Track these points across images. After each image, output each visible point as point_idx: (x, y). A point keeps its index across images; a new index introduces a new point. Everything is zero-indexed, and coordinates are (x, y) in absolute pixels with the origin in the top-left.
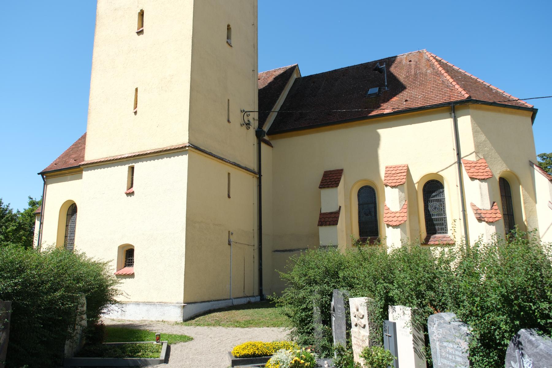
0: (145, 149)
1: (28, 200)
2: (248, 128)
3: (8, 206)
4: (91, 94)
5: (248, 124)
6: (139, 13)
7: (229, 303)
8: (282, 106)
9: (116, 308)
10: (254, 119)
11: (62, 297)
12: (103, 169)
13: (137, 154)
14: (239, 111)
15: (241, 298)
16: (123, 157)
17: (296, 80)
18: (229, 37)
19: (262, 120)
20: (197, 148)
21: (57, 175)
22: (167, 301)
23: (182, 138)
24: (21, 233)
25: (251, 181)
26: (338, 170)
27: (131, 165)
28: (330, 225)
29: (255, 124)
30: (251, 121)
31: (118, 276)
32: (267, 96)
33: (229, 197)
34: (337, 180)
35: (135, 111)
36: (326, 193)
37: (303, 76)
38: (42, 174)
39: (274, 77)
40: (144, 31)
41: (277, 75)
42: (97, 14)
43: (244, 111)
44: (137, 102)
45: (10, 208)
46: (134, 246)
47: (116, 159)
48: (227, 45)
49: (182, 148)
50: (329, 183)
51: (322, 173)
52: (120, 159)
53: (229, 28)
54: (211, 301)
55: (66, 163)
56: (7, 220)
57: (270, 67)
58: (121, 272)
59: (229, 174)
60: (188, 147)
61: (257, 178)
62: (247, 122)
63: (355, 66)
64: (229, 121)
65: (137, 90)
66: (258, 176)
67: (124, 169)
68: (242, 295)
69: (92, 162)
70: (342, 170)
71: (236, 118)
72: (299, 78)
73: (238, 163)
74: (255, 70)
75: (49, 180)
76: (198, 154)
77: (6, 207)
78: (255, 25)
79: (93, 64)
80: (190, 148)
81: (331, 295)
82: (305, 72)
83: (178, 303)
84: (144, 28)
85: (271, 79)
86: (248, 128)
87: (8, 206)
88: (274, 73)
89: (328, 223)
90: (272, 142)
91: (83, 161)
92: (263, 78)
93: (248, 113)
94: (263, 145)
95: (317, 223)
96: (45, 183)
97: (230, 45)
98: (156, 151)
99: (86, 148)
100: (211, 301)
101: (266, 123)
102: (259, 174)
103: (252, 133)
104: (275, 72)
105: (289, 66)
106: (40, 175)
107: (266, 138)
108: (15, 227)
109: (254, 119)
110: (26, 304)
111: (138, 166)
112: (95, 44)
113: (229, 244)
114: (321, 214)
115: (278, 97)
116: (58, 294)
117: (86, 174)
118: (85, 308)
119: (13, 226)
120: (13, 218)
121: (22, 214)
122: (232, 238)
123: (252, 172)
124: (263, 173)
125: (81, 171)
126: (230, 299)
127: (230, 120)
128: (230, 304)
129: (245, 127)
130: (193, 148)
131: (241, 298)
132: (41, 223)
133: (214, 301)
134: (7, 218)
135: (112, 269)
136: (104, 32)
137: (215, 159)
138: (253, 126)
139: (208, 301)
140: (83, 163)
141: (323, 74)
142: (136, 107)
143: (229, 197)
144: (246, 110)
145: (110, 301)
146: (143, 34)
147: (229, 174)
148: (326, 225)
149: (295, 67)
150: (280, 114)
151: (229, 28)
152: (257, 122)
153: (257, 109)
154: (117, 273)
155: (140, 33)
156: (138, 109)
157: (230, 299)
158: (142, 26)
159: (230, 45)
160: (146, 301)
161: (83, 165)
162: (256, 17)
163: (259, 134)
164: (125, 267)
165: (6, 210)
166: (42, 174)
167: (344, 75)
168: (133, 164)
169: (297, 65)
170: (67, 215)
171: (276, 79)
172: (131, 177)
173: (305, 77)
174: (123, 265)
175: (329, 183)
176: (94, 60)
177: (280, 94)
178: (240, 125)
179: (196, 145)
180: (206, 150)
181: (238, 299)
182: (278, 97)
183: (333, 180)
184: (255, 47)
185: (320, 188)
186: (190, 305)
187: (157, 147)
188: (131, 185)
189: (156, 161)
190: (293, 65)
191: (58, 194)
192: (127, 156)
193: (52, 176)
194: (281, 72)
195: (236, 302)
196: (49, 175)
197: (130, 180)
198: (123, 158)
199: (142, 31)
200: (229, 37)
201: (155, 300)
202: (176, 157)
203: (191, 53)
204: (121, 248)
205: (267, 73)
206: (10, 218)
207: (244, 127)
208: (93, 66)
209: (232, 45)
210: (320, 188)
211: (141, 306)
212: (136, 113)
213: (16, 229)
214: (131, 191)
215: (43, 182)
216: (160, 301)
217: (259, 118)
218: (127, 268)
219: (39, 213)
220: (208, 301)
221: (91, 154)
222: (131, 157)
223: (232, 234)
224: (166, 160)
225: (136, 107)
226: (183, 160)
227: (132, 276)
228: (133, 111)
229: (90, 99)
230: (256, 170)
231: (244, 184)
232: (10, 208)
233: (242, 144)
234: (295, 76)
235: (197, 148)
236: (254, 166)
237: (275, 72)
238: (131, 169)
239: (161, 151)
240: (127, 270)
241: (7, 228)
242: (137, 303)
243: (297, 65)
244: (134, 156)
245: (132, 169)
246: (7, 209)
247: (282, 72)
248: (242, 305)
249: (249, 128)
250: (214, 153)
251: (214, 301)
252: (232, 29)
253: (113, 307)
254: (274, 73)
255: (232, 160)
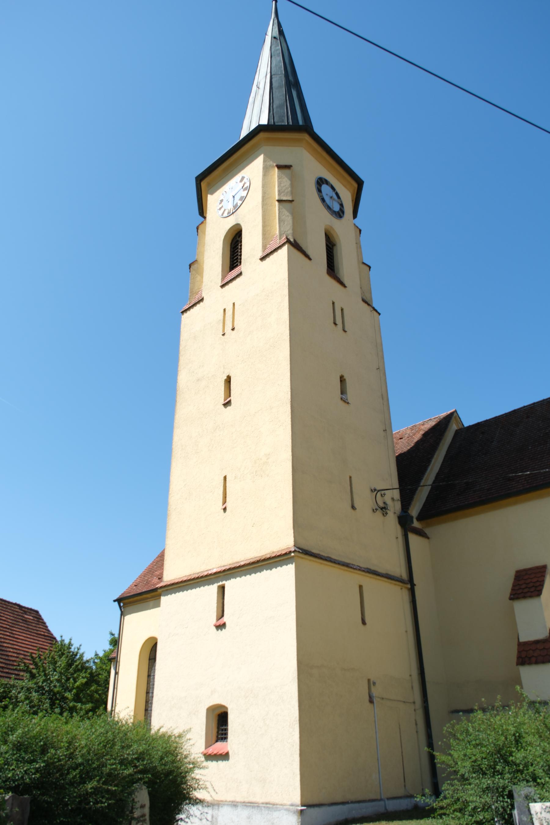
0: (238, 560)
1: (109, 638)
2: (385, 514)
3: (78, 649)
4: (171, 490)
5: (384, 509)
6: (226, 380)
7: (379, 807)
9: (197, 813)
10: (393, 499)
11: (96, 790)
12: (185, 592)
13: (228, 567)
14: (369, 491)
15: (400, 798)
16: (210, 572)
17: (457, 432)
18: (343, 391)
19: (406, 498)
20: (306, 553)
21: (147, 598)
22: (277, 801)
23: (285, 541)
24: (92, 688)
25: (400, 594)
26: (537, 568)
27: (221, 583)
28: (537, 663)
29: (395, 507)
30: (389, 502)
31: (209, 757)
32: (410, 465)
33: (364, 623)
34: (538, 584)
35: (224, 507)
36: (522, 607)
37: (466, 425)
38: (119, 600)
39: (422, 432)
40: (232, 402)
41: (426, 430)
42: (178, 388)
43: (375, 490)
44: (226, 494)
45: (81, 651)
46: (227, 708)
47: (202, 577)
48: (341, 403)
49: (286, 554)
50: (526, 590)
51: (512, 574)
52: (206, 576)
53: (342, 380)
54: (347, 803)
55: (148, 582)
56: (77, 670)
57: (410, 421)
58: (211, 750)
59: (361, 587)
61: (409, 589)
62: (382, 505)
63: (544, 400)
64: (353, 507)
65: (225, 478)
66: (409, 586)
67: (212, 590)
68: (401, 792)
69: (172, 582)
70: (544, 567)
71: (365, 501)
72: (460, 429)
73: (373, 568)
74: (387, 429)
75: (128, 609)
76: (310, 560)
77: (76, 650)
78: (381, 370)
79: (174, 450)
80: (297, 554)
81: (511, 795)
82: (469, 418)
83: (292, 805)
84: (232, 398)
85: (418, 437)
86: (385, 514)
87: (78, 649)
88: (422, 427)
89: (533, 659)
90: (427, 531)
91: (162, 581)
92: (407, 436)
93: (383, 492)
94: (412, 537)
95: (515, 659)
96: (123, 614)
98: (252, 561)
100: (347, 803)
102: (409, 582)
103: (391, 521)
104: (423, 425)
105: (443, 414)
106: (116, 603)
107: (416, 524)
108: (85, 680)
109: (393, 499)
110: (47, 802)
111: (231, 585)
112: (176, 425)
113: (371, 701)
114: (520, 644)
115: (429, 461)
116: (90, 786)
117: (164, 599)
118: (147, 810)
119: (83, 678)
120: (83, 667)
121: (101, 659)
122: (376, 692)
124: (416, 581)
125: (158, 597)
126: (381, 800)
127: (356, 505)
128: (382, 810)
129: (379, 513)
130: (303, 553)
131: (400, 798)
132: (116, 673)
133: (352, 802)
134: (77, 666)
135: (195, 745)
136: (184, 410)
139: (343, 803)
141: (510, 413)
142: (224, 502)
143: (364, 623)
144: (378, 488)
145: (190, 799)
146: (230, 405)
147: (361, 587)
148: (530, 663)
149: (452, 414)
150: (434, 487)
151: (342, 380)
152: (399, 503)
153: (397, 485)
154: (205, 752)
155: (227, 404)
156: (228, 504)
157: (381, 800)
158: (230, 396)
160: (247, 800)
161: (161, 587)
162: (381, 358)
163: (404, 521)
164: (217, 741)
165: (76, 655)
166: (119, 600)
167: (528, 417)
168: (224, 582)
169: (456, 411)
170: (150, 659)
171: (426, 434)
172: (221, 601)
173: (470, 427)
174: (214, 738)
175: (526, 590)
178: (371, 511)
179: (306, 548)
181: (395, 801)
183: (531, 585)
184: (384, 398)
185: (511, 599)
186: (312, 810)
187: (223, 564)
188: (221, 613)
189: (253, 575)
190: (449, 412)
191: (138, 627)
192: (215, 571)
193: (130, 603)
194: (433, 423)
195: (392, 806)
196: (130, 602)
197: (221, 605)
198: (211, 575)
199: (230, 401)
200: (343, 391)
201: (259, 799)
202: (279, 568)
204: (211, 710)
205: (412, 429)
206: (79, 666)
207: (379, 513)
210: (511, 599)
211: (239, 809)
212: (225, 509)
213: (86, 683)
214: (221, 622)
215: (119, 612)
216: (267, 801)
218: (219, 744)
219: (114, 658)
220: (343, 803)
221: (172, 573)
222: (220, 572)
223: (374, 683)
224: (266, 573)
225: (224, 502)
226: (288, 571)
227: (225, 756)
230: (405, 576)
231: (387, 602)
232: (81, 651)
233: (380, 540)
234: (454, 427)
235: (306, 553)
236: (400, 571)
237: (423, 425)
238: (221, 590)
239: (258, 562)
240: (219, 747)
241: (75, 681)
242: (234, 804)
243: (456, 411)
244: (224, 571)
246: (77, 653)
248: (403, 811)
249: (387, 513)
250: (334, 557)
251: (352, 802)
253: (194, 810)
254: (422, 427)
255: (363, 565)
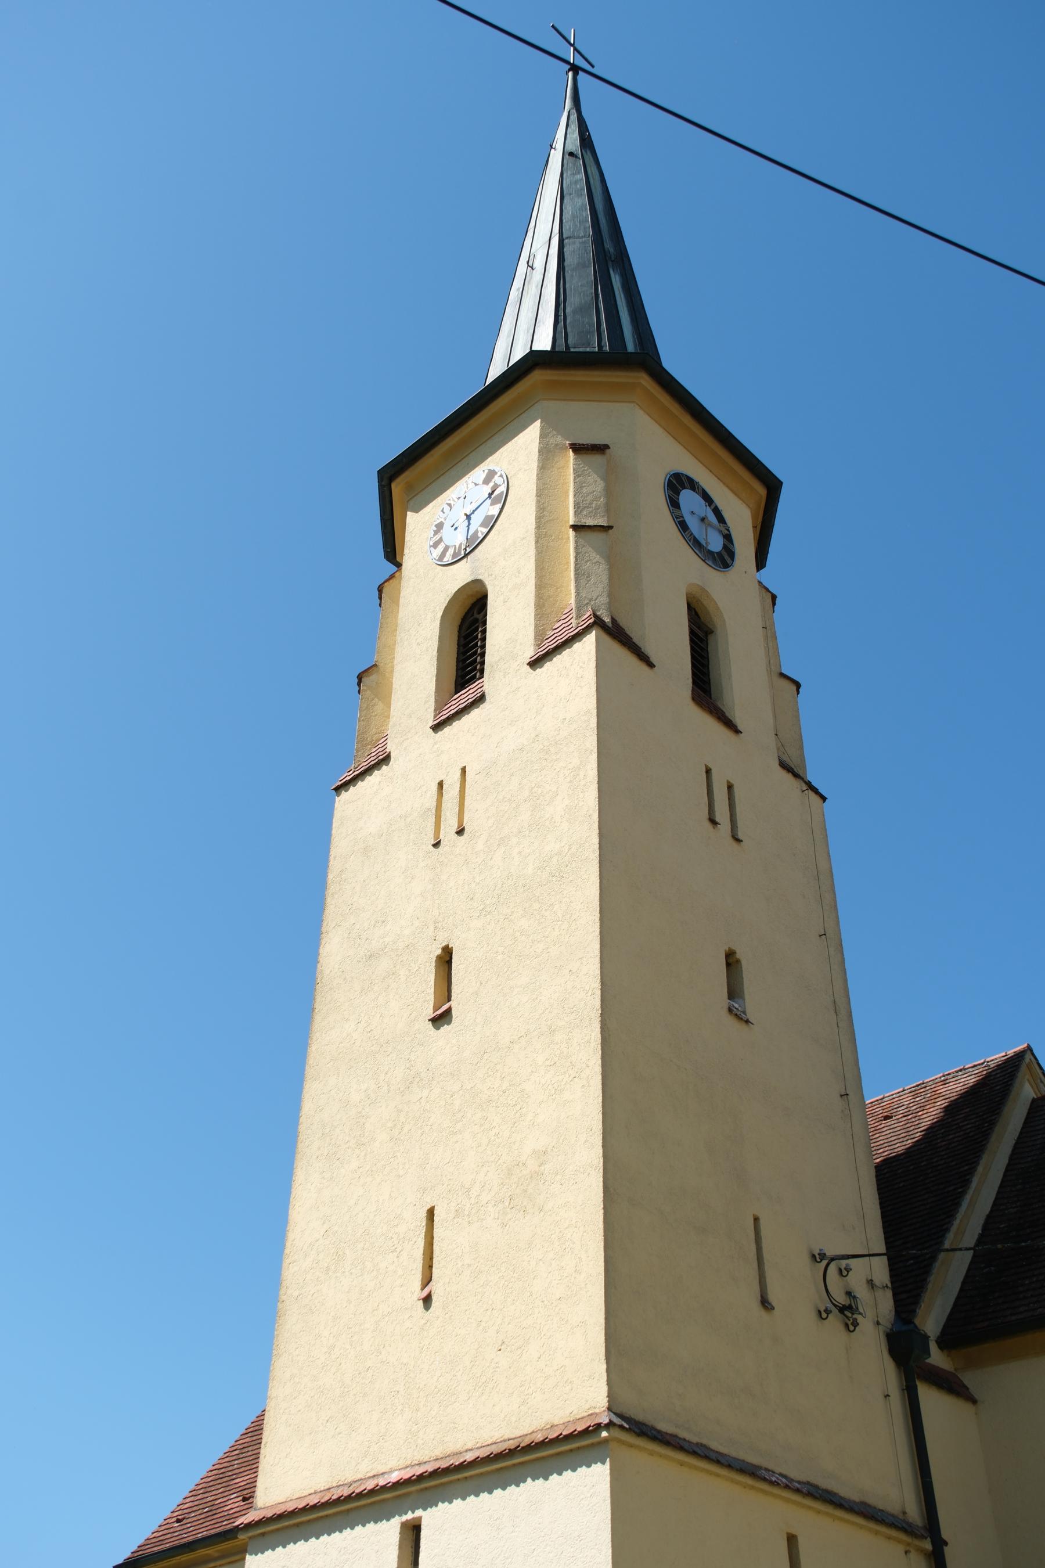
0: (458, 1447)
2: (851, 1326)
4: (288, 1244)
5: (848, 1311)
8: (990, 1220)
10: (871, 1283)
13: (430, 1468)
14: (806, 1259)
16: (382, 1482)
17: (1037, 1106)
18: (734, 991)
19: (908, 1283)
23: (583, 1393)
27: (410, 1516)
29: (878, 1307)
30: (862, 1292)
32: (915, 1188)
39: (942, 1103)
40: (454, 1012)
41: (954, 1096)
43: (823, 1256)
44: (431, 1259)
48: (730, 1021)
49: (586, 1432)
52: (372, 1492)
53: (732, 961)
55: (213, 1510)
59: (792, 1540)
60: (610, 1425)
62: (841, 1299)
64: (765, 1303)
65: (431, 1213)
66: (928, 1546)
69: (279, 1510)
71: (796, 1287)
74: (850, 1090)
76: (652, 1453)
79: (301, 1137)
80: (617, 1433)
85: (931, 1115)
86: (851, 1326)
88: (943, 1089)
90: (969, 1379)
92: (902, 1110)
93: (844, 1263)
94: (929, 1397)
97: (741, 1017)
98: (496, 1449)
99: (262, 1456)
101: (926, 1297)
102: (927, 1531)
103: (870, 1343)
104: (944, 1082)
105: (997, 1057)
107: (937, 1358)
109: (871, 1283)
111: (439, 1520)
112: (310, 1071)
123: (892, 1525)
127: (772, 1298)
130: (630, 1431)
137: (724, 1472)
138: (870, 1313)
140: (251, 1516)
144: (830, 1252)
146: (449, 1023)
147: (792, 1540)
149: (1019, 1056)
151: (732, 961)
152: (889, 1294)
156: (437, 1287)
158: (449, 999)
159: (741, 1017)
161: (249, 1526)
163: (903, 1346)
168: (419, 1513)
169: (1029, 1048)
171: (953, 1109)
176: (302, 1128)
177: (972, 1171)
178: (814, 1315)
179: (640, 1417)
180: (683, 1434)
182: (966, 1183)
184: (841, 1010)
187: (497, 1436)
190: (1011, 1052)
192: (394, 1477)
198: (384, 1488)
199: (449, 1011)
200: (734, 991)
203: (598, 1069)
205: (916, 1091)
208: (301, 1146)
209: (750, 1016)
212: (427, 1301)
217: (892, 1276)
222: (408, 1482)
228: (416, 1292)
229: (286, 1262)
230: (914, 1513)
234: (1026, 1092)
236: (899, 1494)
237: (944, 1082)
238: (411, 1535)
243: (1029, 1048)
244: (421, 1478)
245: (413, 1532)
247: (972, 1080)
249: (856, 1324)
252: (744, 963)
254: (943, 1089)
255: (796, 1474)
